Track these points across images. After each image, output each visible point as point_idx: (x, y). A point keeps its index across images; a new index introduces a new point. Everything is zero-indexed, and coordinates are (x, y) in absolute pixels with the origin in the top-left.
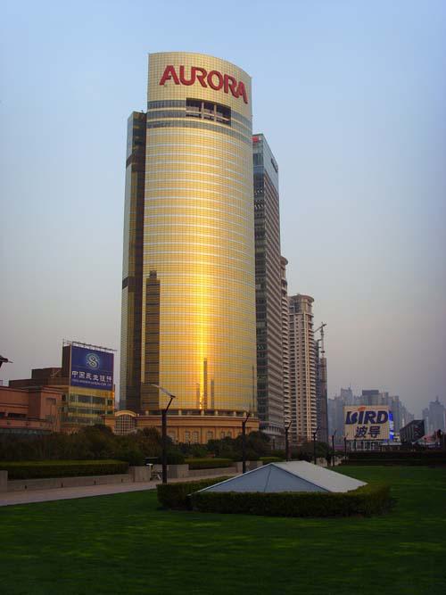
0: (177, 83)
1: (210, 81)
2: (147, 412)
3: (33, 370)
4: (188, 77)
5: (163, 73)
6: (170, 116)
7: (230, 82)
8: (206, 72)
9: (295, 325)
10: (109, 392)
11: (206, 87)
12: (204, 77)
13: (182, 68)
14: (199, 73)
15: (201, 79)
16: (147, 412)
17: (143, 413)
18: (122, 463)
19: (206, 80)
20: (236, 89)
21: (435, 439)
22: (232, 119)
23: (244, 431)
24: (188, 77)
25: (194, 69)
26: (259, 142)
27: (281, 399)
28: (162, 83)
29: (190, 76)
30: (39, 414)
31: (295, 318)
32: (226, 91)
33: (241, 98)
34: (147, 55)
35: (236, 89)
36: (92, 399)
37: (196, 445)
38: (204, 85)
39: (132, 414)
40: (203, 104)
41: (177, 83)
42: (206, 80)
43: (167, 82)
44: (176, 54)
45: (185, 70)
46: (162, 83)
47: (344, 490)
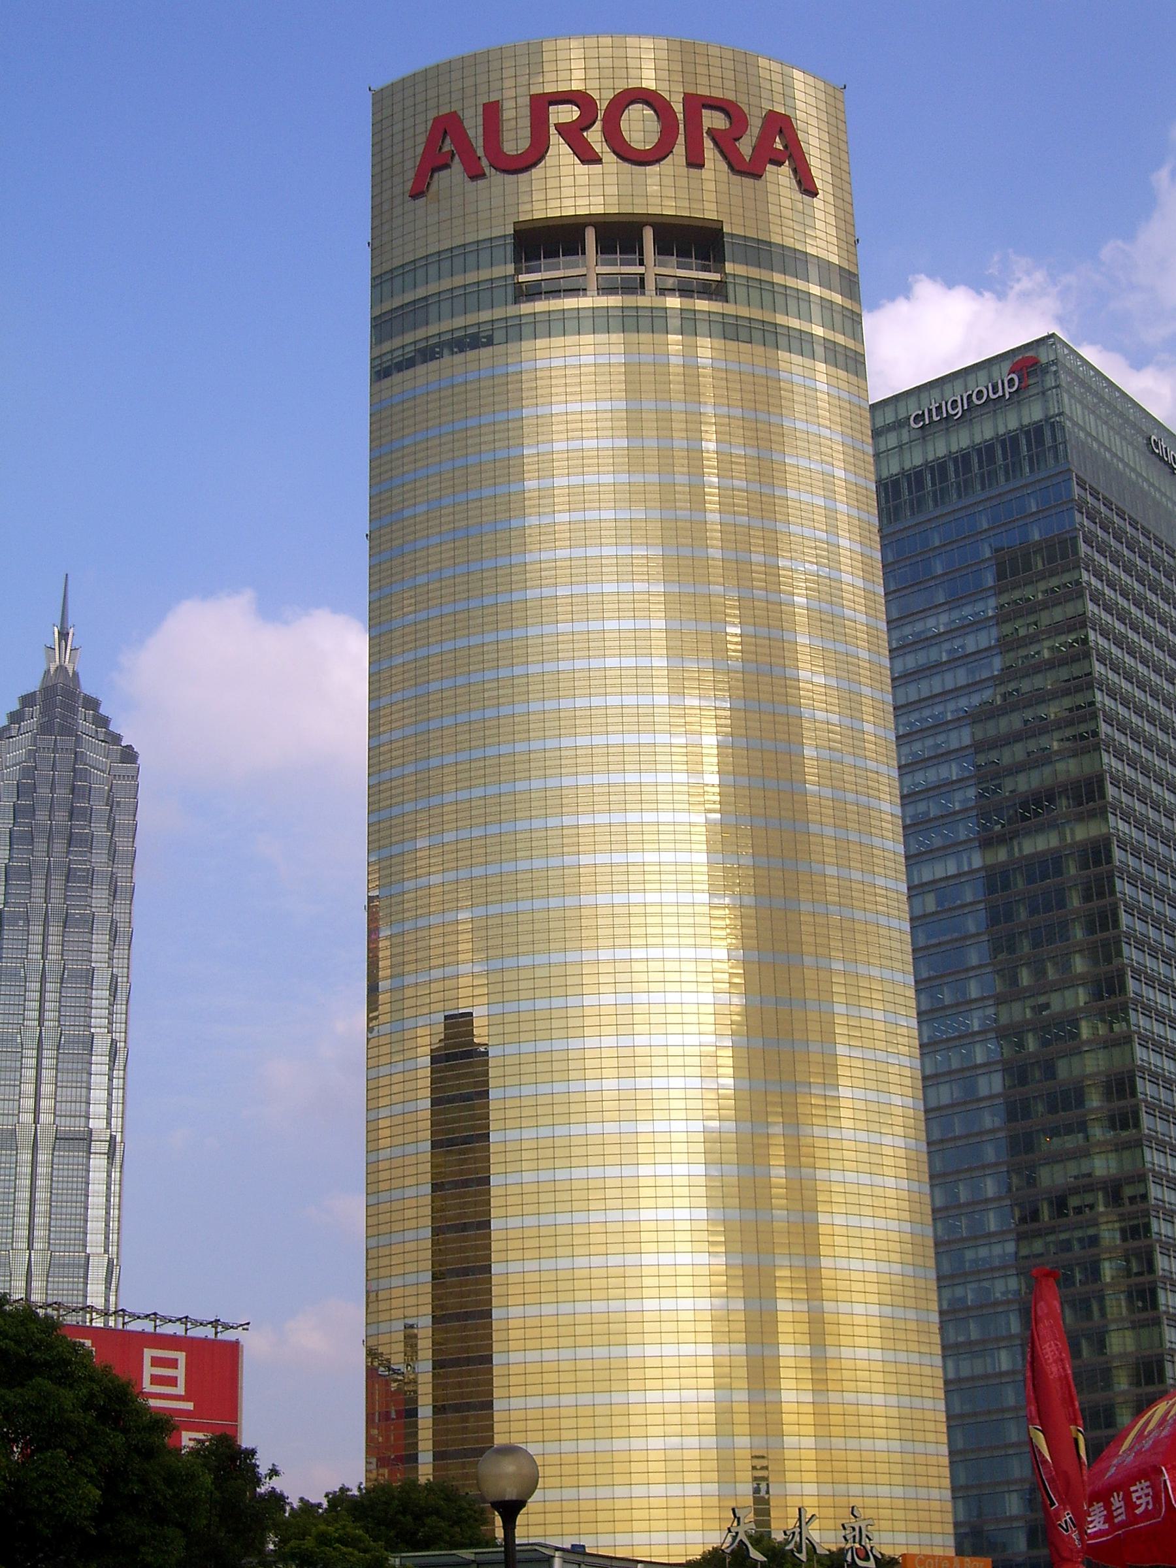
0: (476, 175)
1: (613, 136)
3: (233, 1349)
5: (422, 139)
7: (713, 120)
8: (592, 101)
10: (952, 1339)
11: (597, 160)
12: (585, 123)
13: (492, 112)
14: (567, 114)
15: (573, 134)
18: (680, 116)
19: (595, 136)
20: (746, 147)
21: (441, 1491)
24: (516, 141)
25: (541, 104)
26: (1044, 370)
32: (695, 161)
33: (781, 177)
34: (369, 96)
37: (704, 1556)
38: (588, 157)
40: (648, 235)
42: (595, 136)
43: (442, 179)
45: (508, 114)
47: (471, 133)
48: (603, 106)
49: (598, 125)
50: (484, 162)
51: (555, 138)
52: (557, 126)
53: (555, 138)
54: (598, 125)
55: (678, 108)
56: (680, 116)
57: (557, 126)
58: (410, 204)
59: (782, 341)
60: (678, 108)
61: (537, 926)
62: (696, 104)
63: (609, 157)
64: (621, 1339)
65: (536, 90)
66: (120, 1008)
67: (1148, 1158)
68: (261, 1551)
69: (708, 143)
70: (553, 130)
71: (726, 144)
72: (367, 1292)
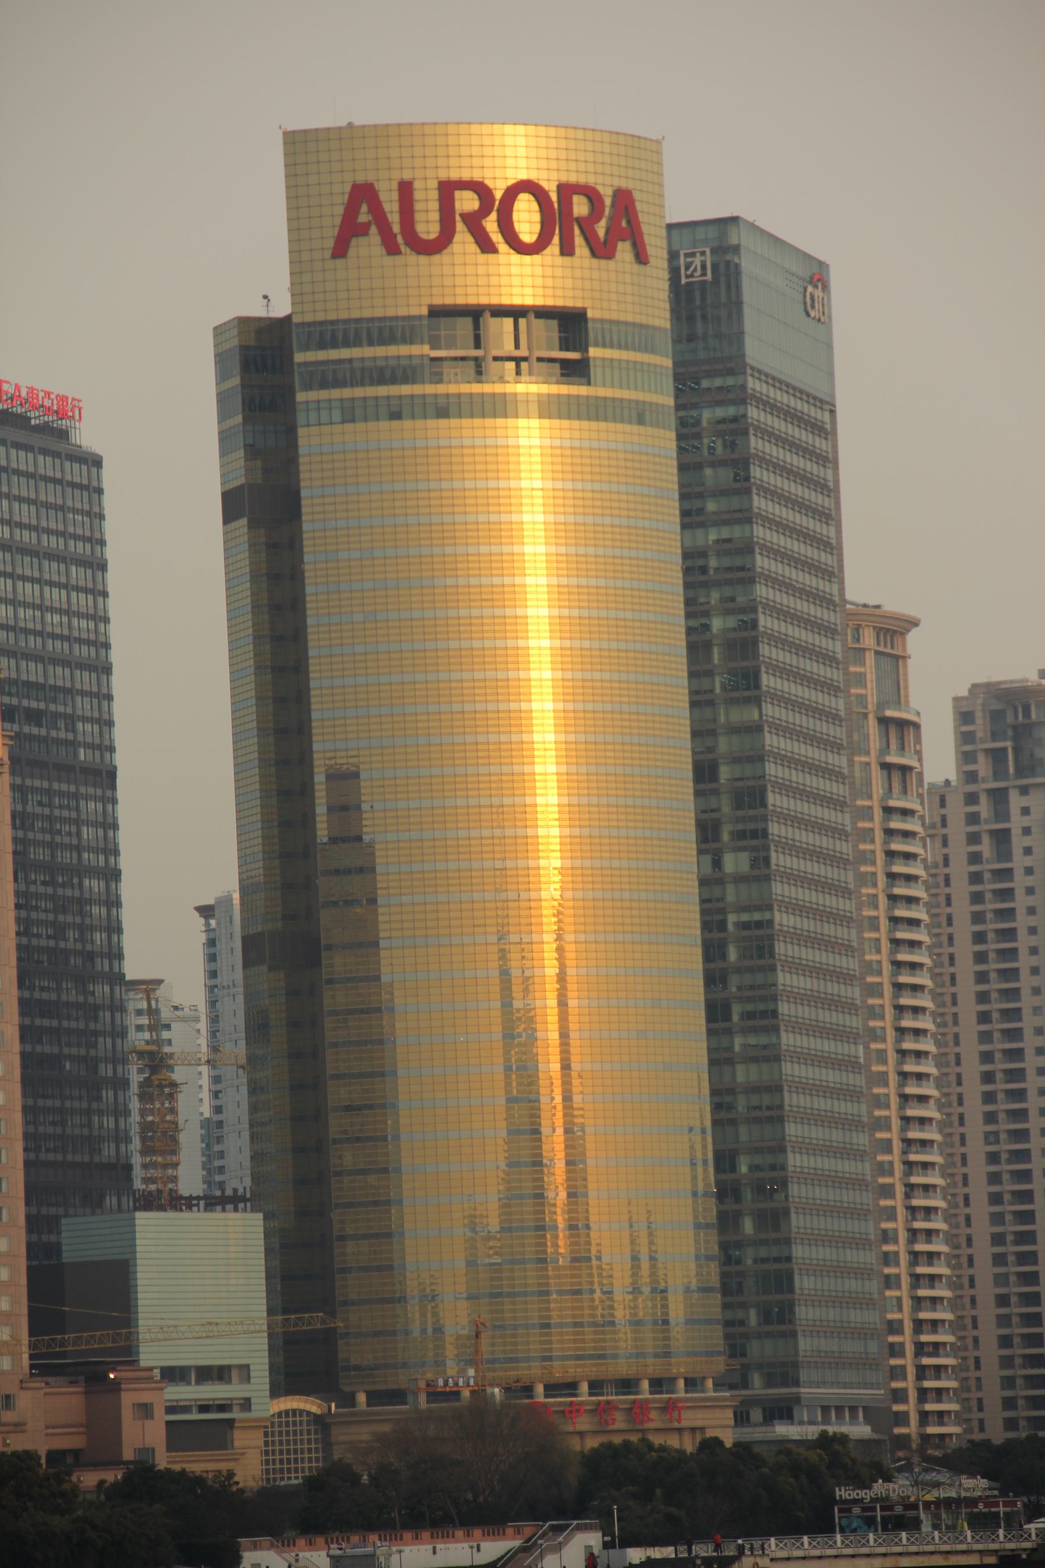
2: (362, 1398)
4: (428, 227)
6: (383, 341)
9: (1018, 843)
12: (485, 209)
13: (406, 189)
14: (467, 202)
15: (474, 222)
16: (362, 1398)
17: (349, 1400)
18: (556, 205)
19: (491, 224)
20: (601, 229)
22: (593, 352)
23: (102, 955)
24: (428, 227)
25: (447, 189)
27: (866, 1198)
28: (340, 250)
29: (435, 216)
30: (120, 1452)
31: (1016, 800)
32: (567, 250)
33: (624, 250)
35: (601, 229)
36: (315, 1321)
38: (487, 246)
39: (311, 1405)
41: (392, 249)
42: (491, 224)
44: (382, 133)
45: (418, 195)
46: (340, 250)
47: (387, 207)
48: (498, 195)
49: (494, 216)
50: (400, 239)
51: (460, 226)
52: (462, 215)
53: (460, 226)
54: (494, 216)
55: (554, 197)
56: (556, 205)
57: (462, 215)
58: (330, 264)
59: (521, 408)
60: (554, 197)
61: (431, 476)
62: (566, 190)
63: (503, 247)
64: (509, 760)
65: (443, 175)
66: (11, 1428)
67: (768, 741)
68: (369, 1475)
69: (577, 231)
70: (458, 218)
71: (587, 226)
72: (411, 124)
